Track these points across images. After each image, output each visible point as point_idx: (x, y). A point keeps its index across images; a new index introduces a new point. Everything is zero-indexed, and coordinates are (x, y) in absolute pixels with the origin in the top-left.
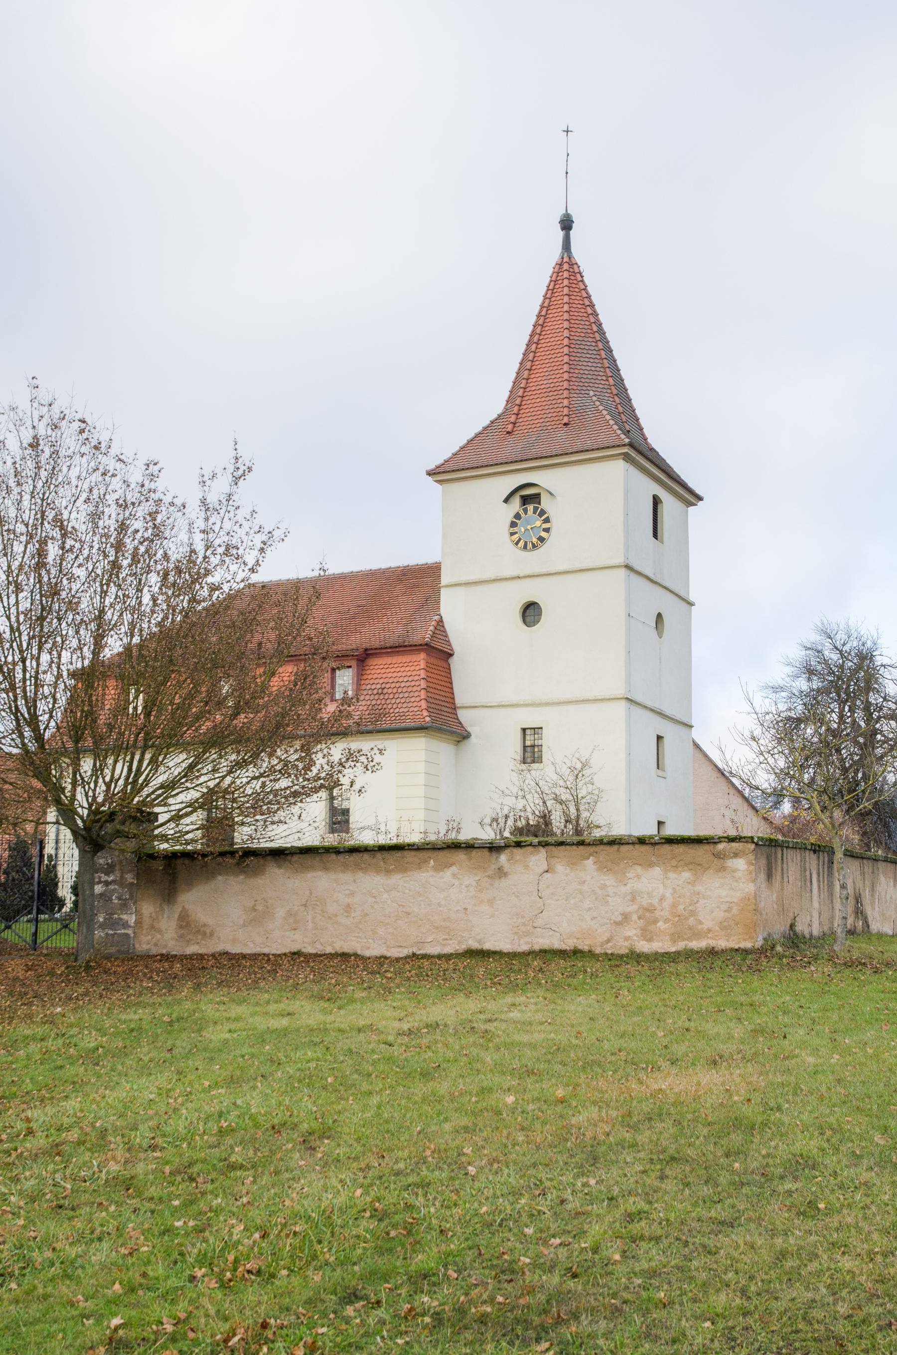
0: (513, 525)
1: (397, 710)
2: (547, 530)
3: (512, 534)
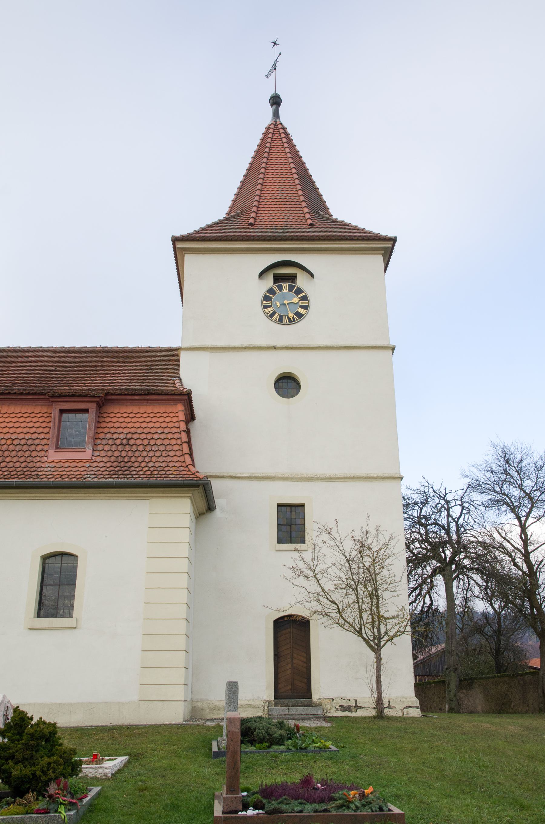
0: (266, 298)
1: (151, 464)
2: (306, 307)
3: (265, 307)
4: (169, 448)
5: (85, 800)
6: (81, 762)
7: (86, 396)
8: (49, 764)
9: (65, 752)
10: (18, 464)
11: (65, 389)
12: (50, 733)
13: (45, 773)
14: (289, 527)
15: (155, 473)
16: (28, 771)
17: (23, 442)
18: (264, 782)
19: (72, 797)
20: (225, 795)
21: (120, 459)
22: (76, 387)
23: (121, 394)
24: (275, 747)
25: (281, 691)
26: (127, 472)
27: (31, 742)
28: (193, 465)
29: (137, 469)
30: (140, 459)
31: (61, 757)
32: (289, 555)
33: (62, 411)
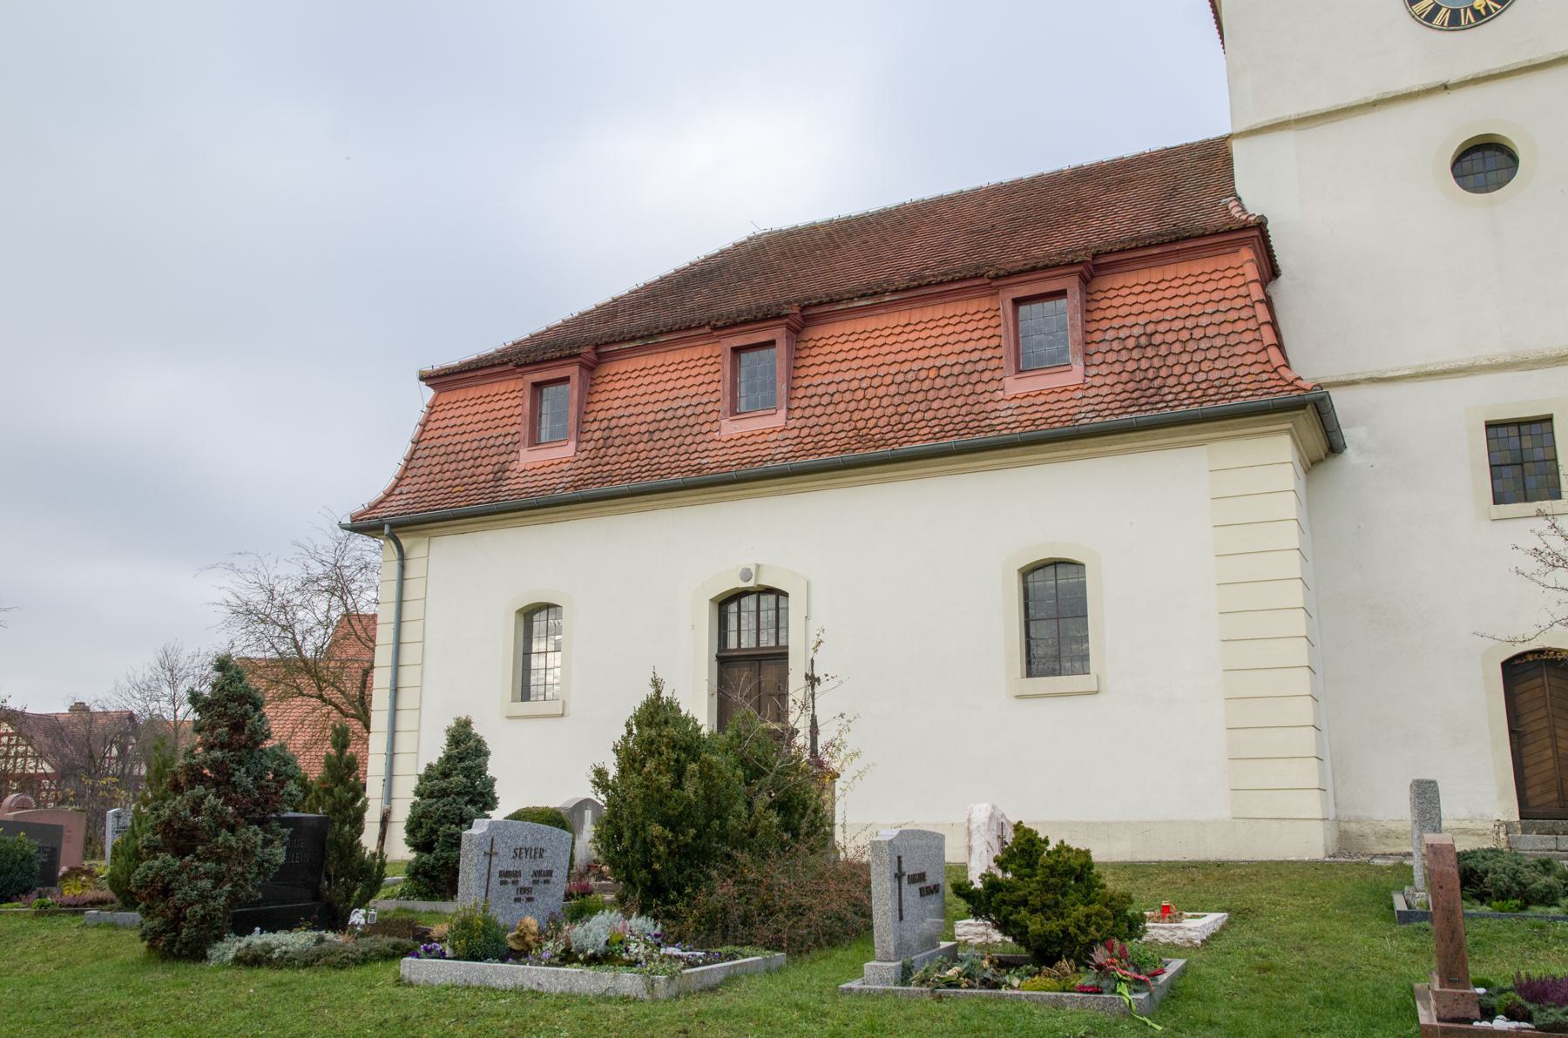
1: (1201, 377)
4: (1233, 339)
5: (1163, 978)
6: (1143, 919)
7: (1057, 266)
8: (1088, 916)
9: (1112, 899)
10: (954, 411)
11: (1017, 261)
12: (1082, 866)
13: (1083, 931)
14: (1517, 469)
15: (1211, 391)
16: (1054, 926)
17: (956, 370)
18: (1523, 973)
19: (1138, 970)
20: (1437, 988)
21: (1139, 375)
22: (1036, 252)
23: (1122, 251)
24: (1538, 910)
25: (1533, 803)
26: (1157, 398)
27: (1052, 880)
28: (1288, 366)
29: (1174, 390)
30: (1178, 370)
31: (1107, 906)
32: (1525, 526)
33: (1017, 302)
